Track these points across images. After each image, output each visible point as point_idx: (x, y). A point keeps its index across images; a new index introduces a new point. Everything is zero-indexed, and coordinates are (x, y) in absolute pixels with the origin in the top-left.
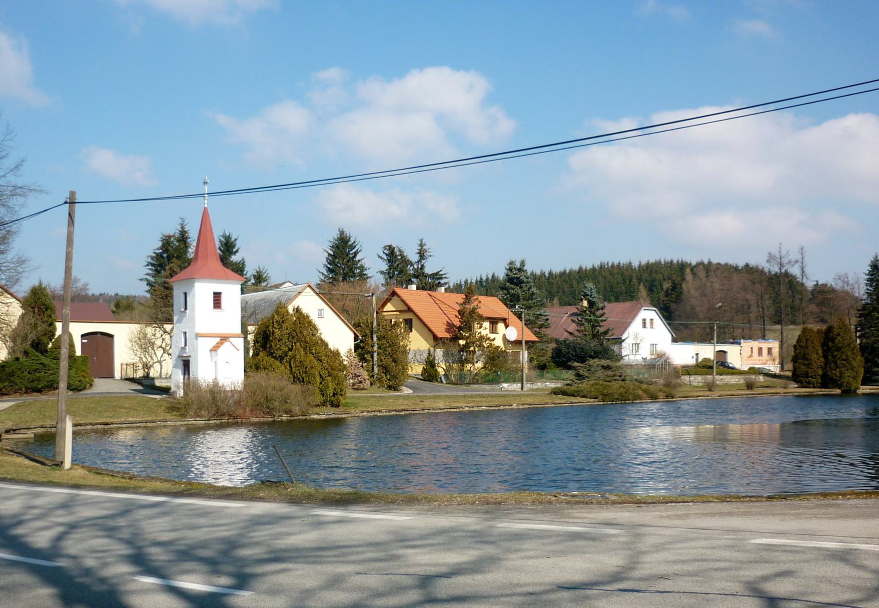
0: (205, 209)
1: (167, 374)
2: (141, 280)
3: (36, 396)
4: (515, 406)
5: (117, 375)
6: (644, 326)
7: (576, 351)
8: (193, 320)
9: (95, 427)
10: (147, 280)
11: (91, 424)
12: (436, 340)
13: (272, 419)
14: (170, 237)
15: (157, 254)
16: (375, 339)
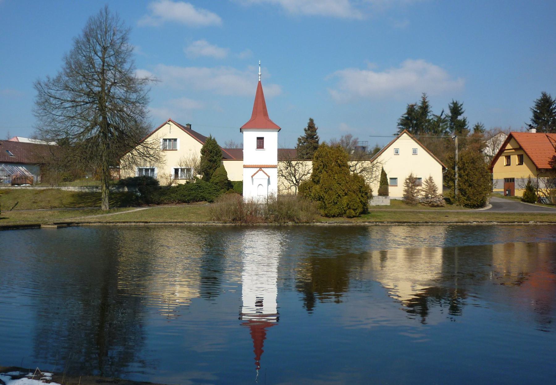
3: (186, 205)
4: (531, 223)
11: (134, 222)
12: (540, 172)
13: (279, 225)
14: (413, 106)
16: (456, 169)
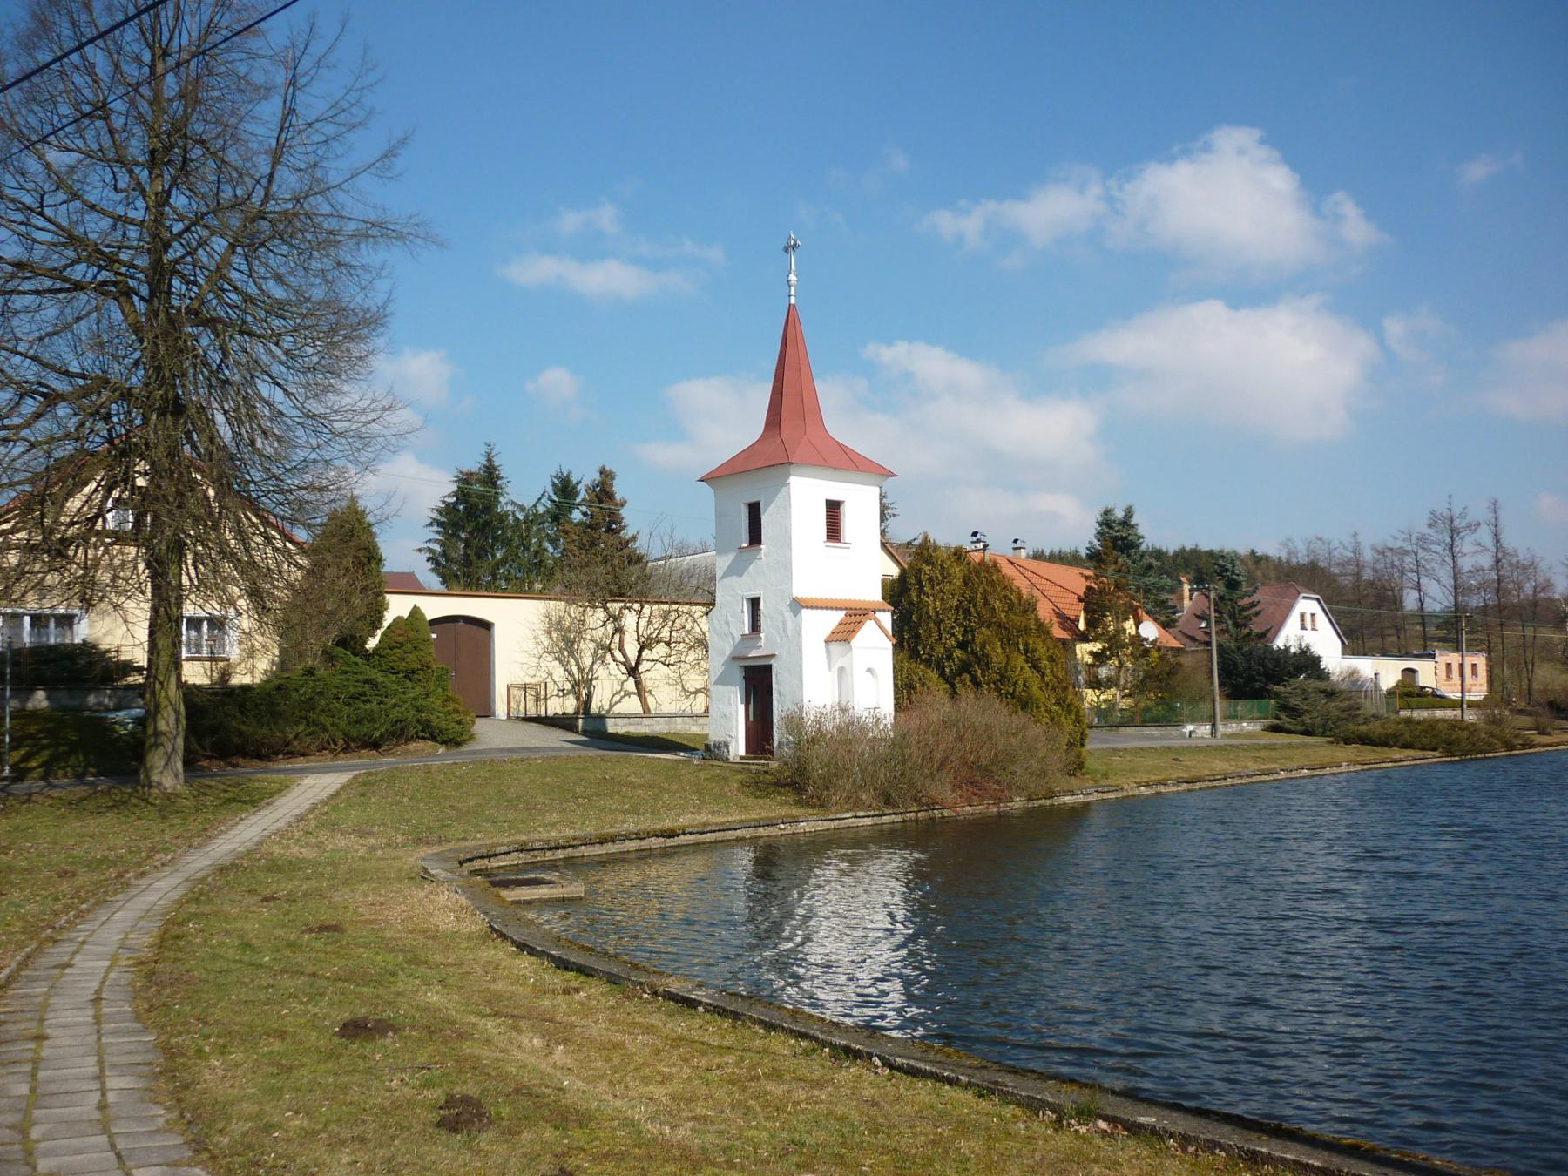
0: (791, 309)
1: (601, 708)
2: (420, 550)
5: (500, 709)
6: (1303, 627)
7: (1264, 666)
8: (786, 567)
9: (645, 844)
10: (429, 549)
15: (448, 505)
